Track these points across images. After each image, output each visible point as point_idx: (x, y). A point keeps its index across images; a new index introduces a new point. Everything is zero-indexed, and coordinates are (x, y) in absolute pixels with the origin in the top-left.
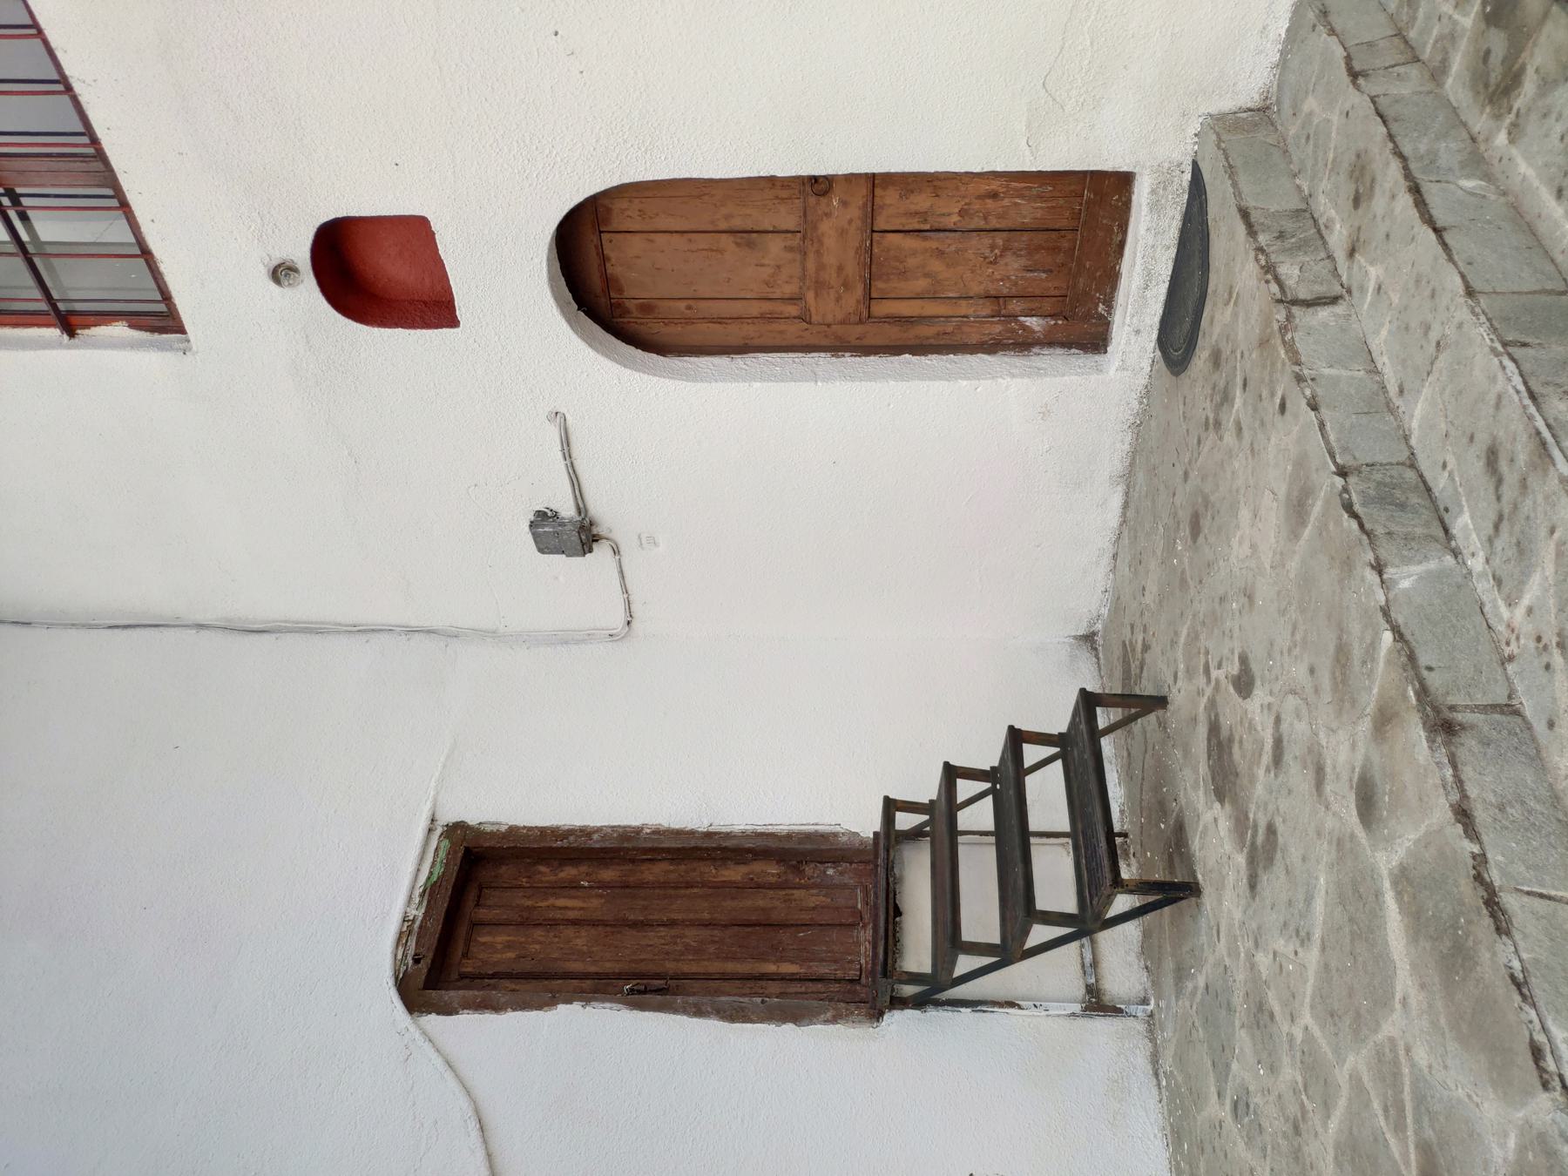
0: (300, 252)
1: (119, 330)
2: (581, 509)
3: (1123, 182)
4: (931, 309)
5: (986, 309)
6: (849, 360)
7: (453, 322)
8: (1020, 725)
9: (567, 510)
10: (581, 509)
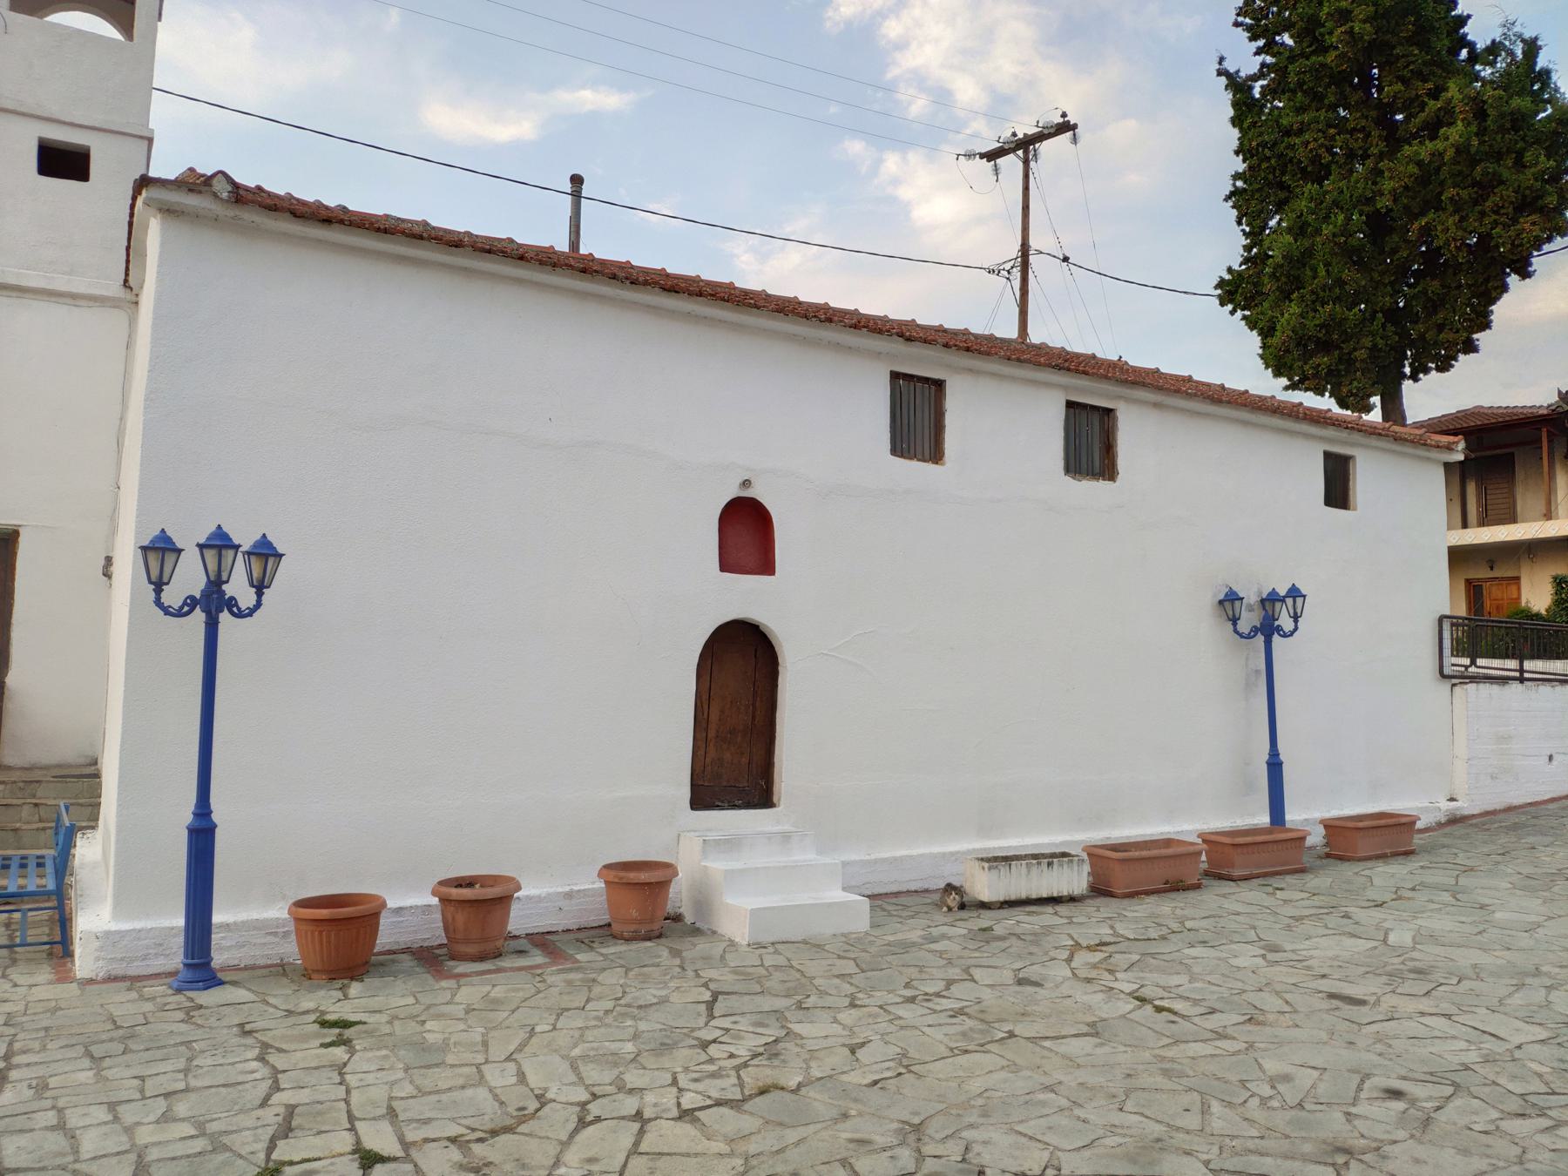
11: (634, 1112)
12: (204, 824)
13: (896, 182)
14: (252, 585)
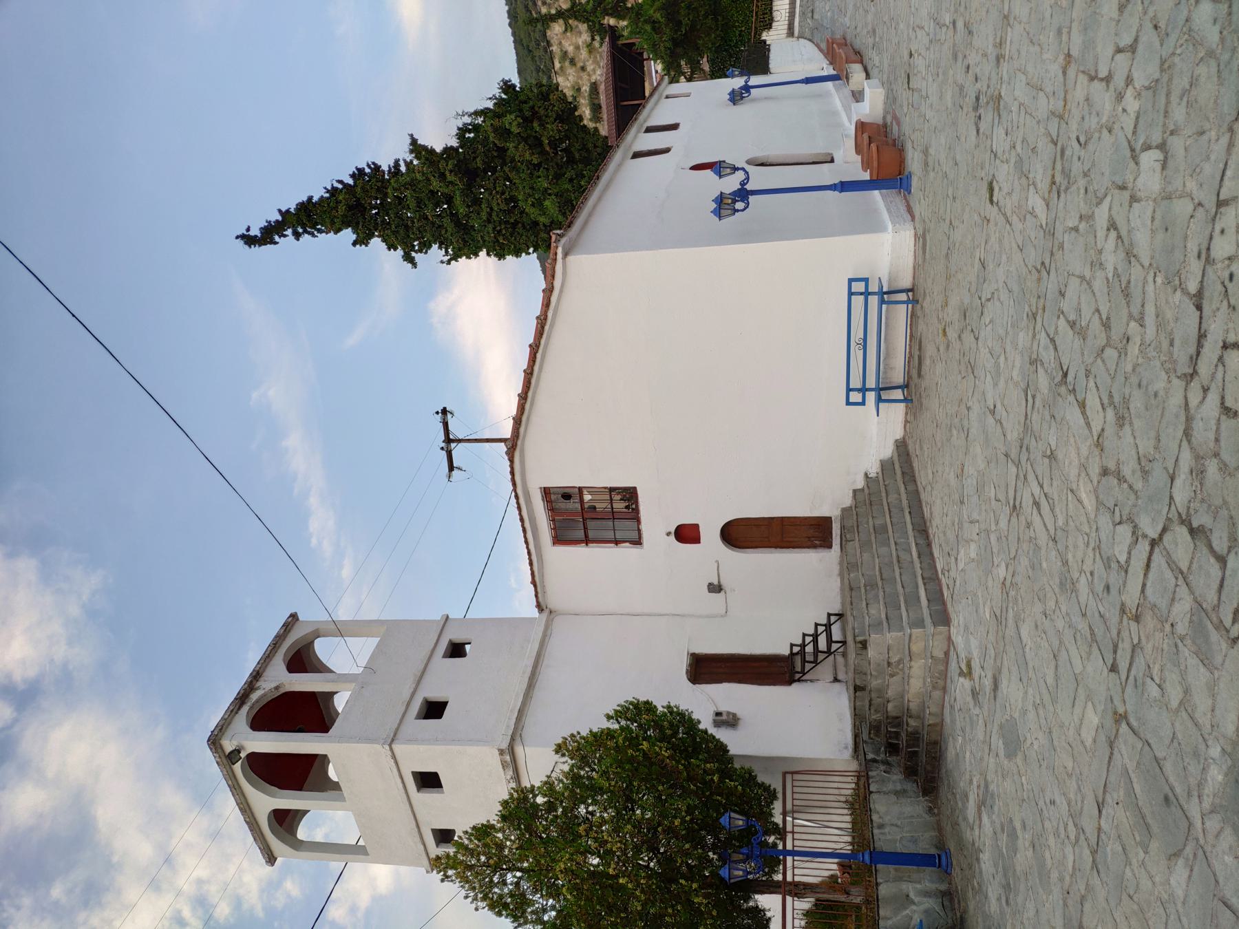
0: (673, 530)
1: (627, 544)
2: (719, 582)
3: (831, 518)
4: (796, 539)
5: (807, 539)
6: (778, 549)
7: (699, 543)
8: (818, 622)
9: (716, 582)
10: (719, 582)
11: (1113, 673)
12: (839, 186)
13: (353, 910)
14: (734, 214)
